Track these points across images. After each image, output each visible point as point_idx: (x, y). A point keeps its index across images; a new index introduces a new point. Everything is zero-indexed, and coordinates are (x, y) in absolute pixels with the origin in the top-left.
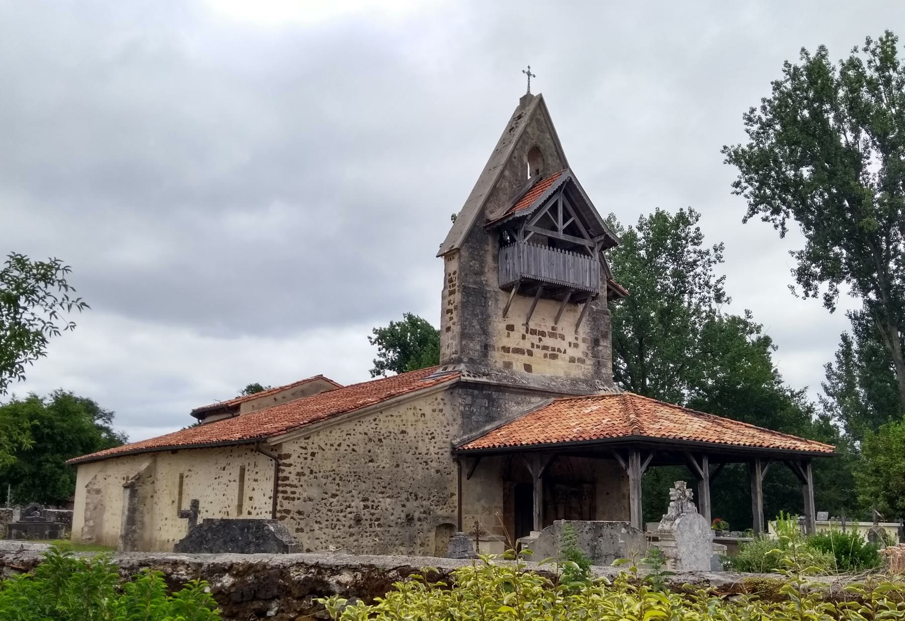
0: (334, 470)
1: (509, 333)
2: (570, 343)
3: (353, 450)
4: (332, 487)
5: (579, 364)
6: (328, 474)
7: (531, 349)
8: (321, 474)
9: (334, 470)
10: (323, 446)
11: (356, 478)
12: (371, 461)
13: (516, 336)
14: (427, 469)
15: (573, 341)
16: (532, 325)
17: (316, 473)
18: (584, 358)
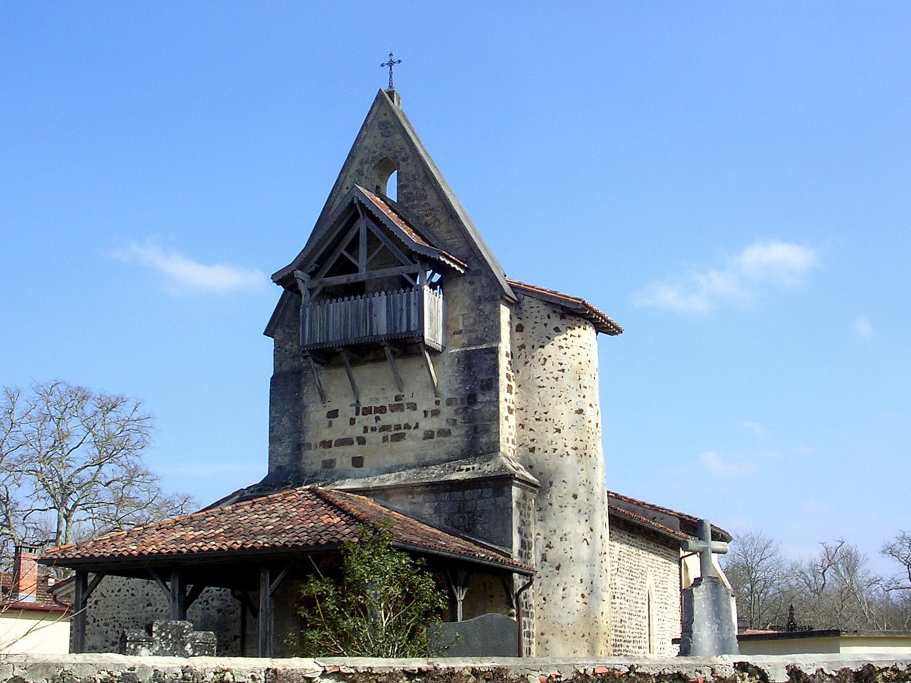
0: (114, 617)
1: (330, 423)
2: (425, 413)
3: (133, 595)
4: (112, 635)
5: (441, 438)
6: (108, 621)
7: (363, 435)
8: (103, 622)
9: (114, 617)
10: (105, 593)
11: (134, 624)
12: (149, 605)
13: (341, 422)
14: (208, 609)
15: (431, 406)
16: (365, 403)
17: (98, 621)
18: (450, 427)
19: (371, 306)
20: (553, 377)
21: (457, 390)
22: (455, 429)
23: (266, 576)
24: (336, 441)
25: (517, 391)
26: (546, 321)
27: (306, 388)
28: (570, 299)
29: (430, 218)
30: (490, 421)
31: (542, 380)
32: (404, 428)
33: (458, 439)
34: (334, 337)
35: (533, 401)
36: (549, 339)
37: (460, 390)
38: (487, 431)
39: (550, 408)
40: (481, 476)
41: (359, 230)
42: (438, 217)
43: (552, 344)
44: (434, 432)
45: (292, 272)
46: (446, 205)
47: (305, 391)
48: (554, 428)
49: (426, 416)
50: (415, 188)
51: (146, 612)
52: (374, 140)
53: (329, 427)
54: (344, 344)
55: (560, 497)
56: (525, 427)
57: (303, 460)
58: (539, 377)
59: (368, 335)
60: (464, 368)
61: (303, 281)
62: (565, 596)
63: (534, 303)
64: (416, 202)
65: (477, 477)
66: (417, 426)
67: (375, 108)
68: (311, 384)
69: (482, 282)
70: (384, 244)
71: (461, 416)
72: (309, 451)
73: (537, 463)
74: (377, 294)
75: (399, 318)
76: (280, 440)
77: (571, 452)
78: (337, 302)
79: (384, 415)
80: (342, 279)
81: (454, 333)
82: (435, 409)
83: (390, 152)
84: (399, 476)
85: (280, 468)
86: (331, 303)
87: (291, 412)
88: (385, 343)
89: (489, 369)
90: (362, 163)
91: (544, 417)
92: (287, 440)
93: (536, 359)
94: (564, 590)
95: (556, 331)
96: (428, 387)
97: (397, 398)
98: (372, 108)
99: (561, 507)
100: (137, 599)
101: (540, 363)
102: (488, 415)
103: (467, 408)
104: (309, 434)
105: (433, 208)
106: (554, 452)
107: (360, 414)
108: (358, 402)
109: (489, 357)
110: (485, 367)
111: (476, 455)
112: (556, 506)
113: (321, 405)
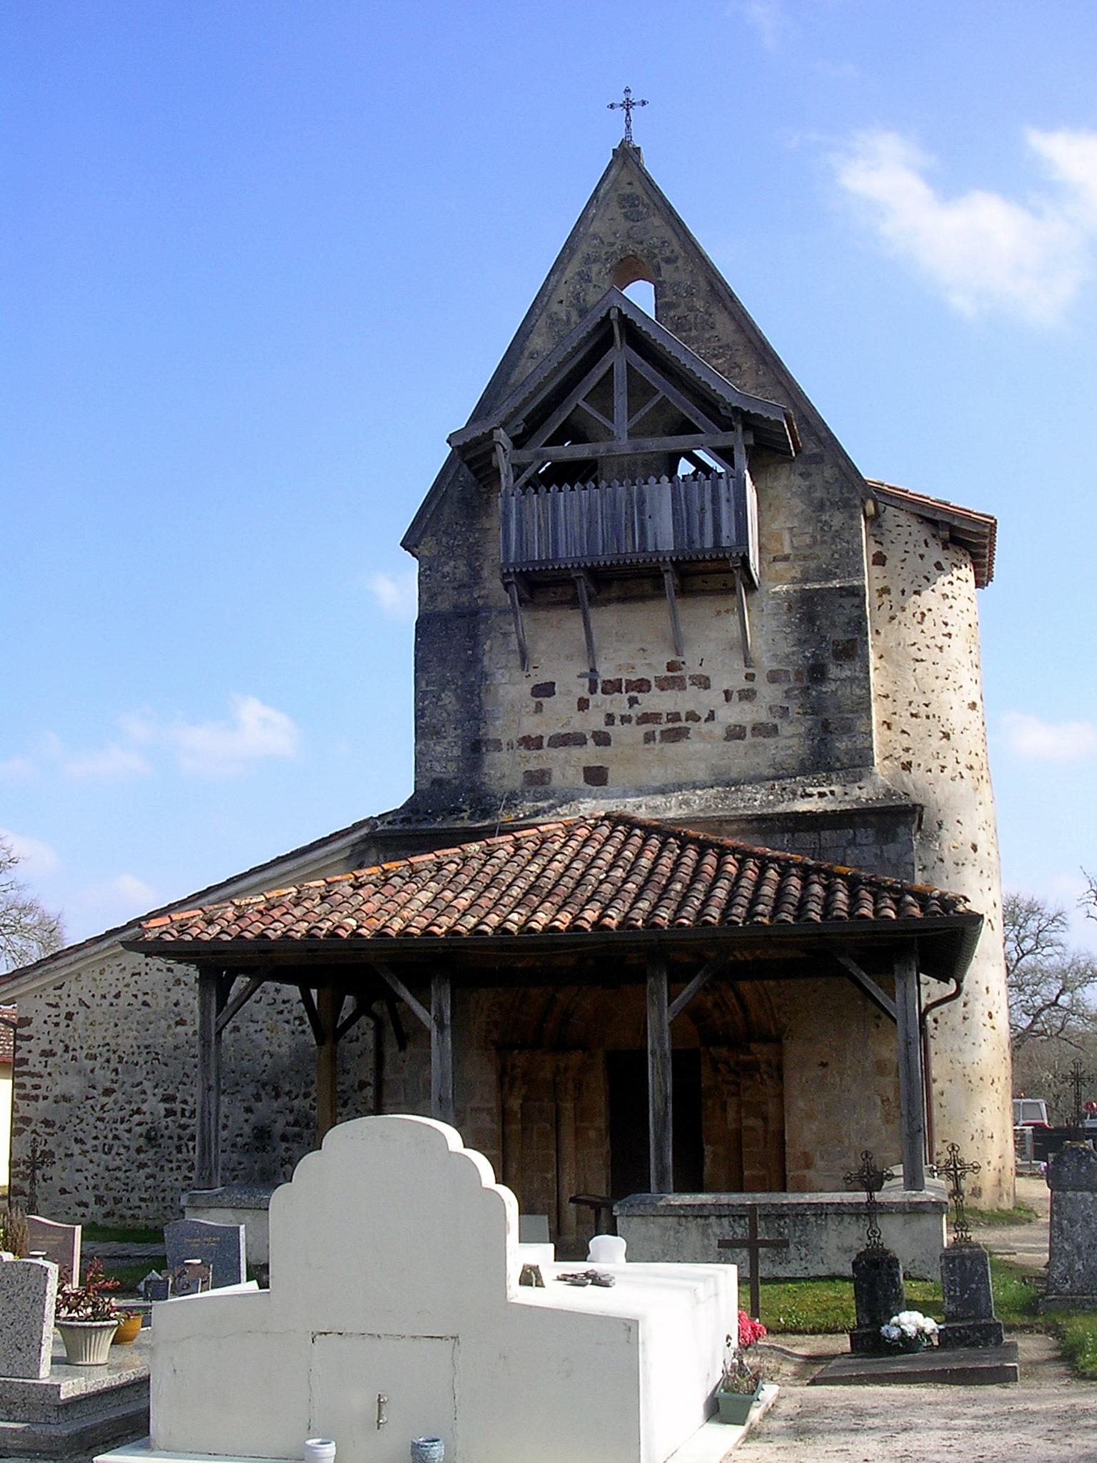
0: (108, 1044)
2: (728, 695)
3: (145, 1004)
5: (760, 739)
8: (85, 1052)
11: (149, 1058)
16: (606, 672)
17: (74, 1050)
18: (776, 721)
19: (642, 502)
20: (936, 646)
21: (787, 656)
22: (785, 724)
23: (659, 985)
24: (551, 738)
25: (878, 666)
26: (923, 550)
27: (488, 643)
28: (973, 516)
29: (720, 361)
30: (852, 712)
31: (919, 650)
32: (687, 720)
33: (795, 741)
34: (570, 551)
35: (906, 684)
36: (928, 580)
37: (795, 658)
38: (848, 729)
39: (931, 697)
40: (855, 807)
41: (612, 368)
42: (737, 360)
43: (933, 590)
44: (745, 728)
45: (491, 431)
46: (755, 341)
47: (486, 647)
48: (941, 732)
49: (728, 699)
50: (691, 309)
51: (175, 1035)
52: (611, 224)
53: (536, 712)
54: (589, 565)
55: (954, 847)
56: (893, 727)
57: (486, 770)
58: (915, 644)
59: (637, 550)
60: (800, 619)
61: (504, 450)
62: (967, 1016)
63: (903, 518)
64: (694, 333)
65: (848, 807)
66: (711, 717)
67: (613, 172)
68: (498, 635)
69: (825, 475)
70: (662, 393)
71: (796, 701)
72: (497, 754)
73: (916, 789)
74: (652, 480)
75: (698, 524)
76: (438, 733)
77: (966, 773)
78: (573, 489)
79: (646, 695)
80: (568, 451)
81: (774, 558)
82: (746, 687)
83: (641, 247)
84: (686, 802)
85: (437, 782)
86: (560, 491)
87: (460, 683)
88: (670, 567)
89: (849, 623)
90: (588, 260)
91: (923, 711)
92: (452, 733)
93: (909, 612)
94: (965, 1005)
95: (938, 569)
96: (731, 649)
97: (671, 667)
98: (608, 170)
99: (957, 864)
100: (155, 1013)
101: (915, 621)
102: (849, 702)
103: (808, 688)
104: (497, 723)
105: (728, 345)
106: (942, 771)
107: (599, 690)
108: (593, 670)
109: (847, 602)
110: (840, 620)
111: (830, 769)
112: (949, 863)
113: (518, 674)
